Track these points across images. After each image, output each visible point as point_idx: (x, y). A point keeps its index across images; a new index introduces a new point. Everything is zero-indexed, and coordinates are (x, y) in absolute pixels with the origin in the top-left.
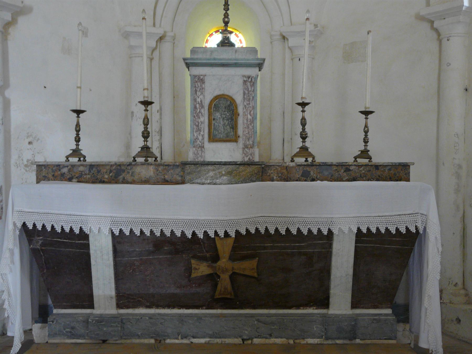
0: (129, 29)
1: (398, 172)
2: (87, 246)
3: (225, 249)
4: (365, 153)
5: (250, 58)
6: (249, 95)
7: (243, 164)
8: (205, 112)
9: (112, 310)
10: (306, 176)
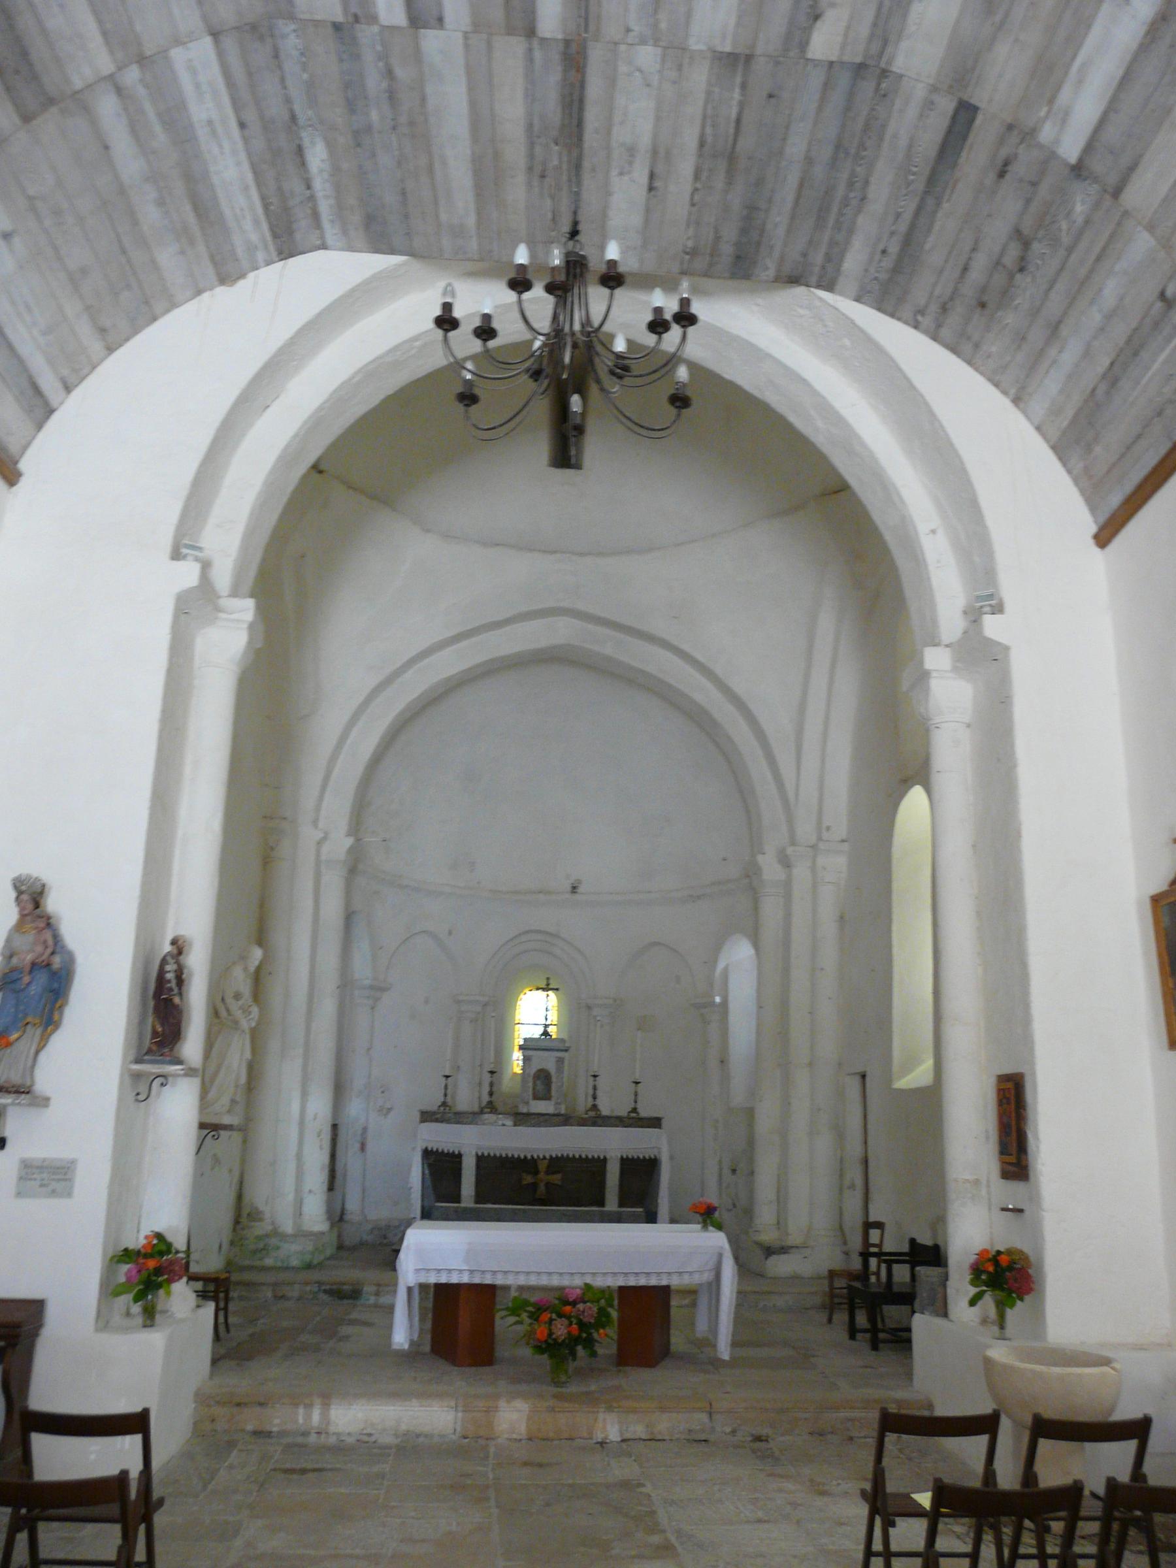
0: (461, 998)
1: (655, 1123)
2: (460, 1163)
3: (542, 1166)
4: (634, 1110)
5: (561, 1046)
6: (560, 1069)
7: (554, 1115)
8: (531, 1079)
9: (472, 1205)
10: (594, 1124)
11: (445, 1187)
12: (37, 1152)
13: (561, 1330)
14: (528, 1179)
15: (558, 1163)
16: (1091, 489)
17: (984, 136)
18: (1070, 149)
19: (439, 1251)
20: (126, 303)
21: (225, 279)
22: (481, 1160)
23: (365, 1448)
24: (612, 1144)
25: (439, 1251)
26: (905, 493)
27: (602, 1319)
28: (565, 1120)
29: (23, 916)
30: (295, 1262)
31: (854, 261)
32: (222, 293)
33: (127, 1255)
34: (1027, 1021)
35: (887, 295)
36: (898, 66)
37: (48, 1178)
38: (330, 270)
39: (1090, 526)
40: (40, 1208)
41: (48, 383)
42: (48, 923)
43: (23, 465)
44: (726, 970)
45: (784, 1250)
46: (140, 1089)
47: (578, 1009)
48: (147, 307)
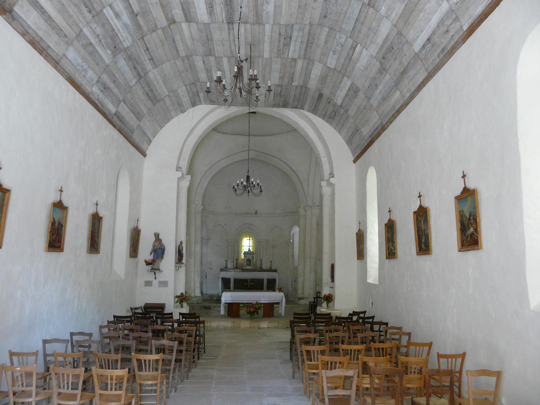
1: (275, 271)
3: (249, 281)
11: (226, 285)
12: (161, 280)
13: (252, 310)
14: (246, 284)
15: (252, 280)
16: (353, 152)
17: (324, 100)
18: (339, 102)
19: (227, 297)
20: (164, 119)
21: (183, 112)
22: (235, 279)
23: (218, 328)
24: (265, 276)
25: (227, 297)
26: (319, 149)
27: (260, 308)
28: (254, 270)
29: (156, 240)
30: (195, 302)
31: (306, 107)
32: (182, 116)
33: (177, 297)
34: (335, 254)
35: (314, 111)
36: (309, 86)
37: (164, 284)
38: (203, 109)
39: (352, 159)
40: (163, 289)
41: (149, 134)
42: (160, 241)
44: (293, 233)
45: (303, 298)
46: (177, 269)
47: (257, 243)
48: (167, 119)
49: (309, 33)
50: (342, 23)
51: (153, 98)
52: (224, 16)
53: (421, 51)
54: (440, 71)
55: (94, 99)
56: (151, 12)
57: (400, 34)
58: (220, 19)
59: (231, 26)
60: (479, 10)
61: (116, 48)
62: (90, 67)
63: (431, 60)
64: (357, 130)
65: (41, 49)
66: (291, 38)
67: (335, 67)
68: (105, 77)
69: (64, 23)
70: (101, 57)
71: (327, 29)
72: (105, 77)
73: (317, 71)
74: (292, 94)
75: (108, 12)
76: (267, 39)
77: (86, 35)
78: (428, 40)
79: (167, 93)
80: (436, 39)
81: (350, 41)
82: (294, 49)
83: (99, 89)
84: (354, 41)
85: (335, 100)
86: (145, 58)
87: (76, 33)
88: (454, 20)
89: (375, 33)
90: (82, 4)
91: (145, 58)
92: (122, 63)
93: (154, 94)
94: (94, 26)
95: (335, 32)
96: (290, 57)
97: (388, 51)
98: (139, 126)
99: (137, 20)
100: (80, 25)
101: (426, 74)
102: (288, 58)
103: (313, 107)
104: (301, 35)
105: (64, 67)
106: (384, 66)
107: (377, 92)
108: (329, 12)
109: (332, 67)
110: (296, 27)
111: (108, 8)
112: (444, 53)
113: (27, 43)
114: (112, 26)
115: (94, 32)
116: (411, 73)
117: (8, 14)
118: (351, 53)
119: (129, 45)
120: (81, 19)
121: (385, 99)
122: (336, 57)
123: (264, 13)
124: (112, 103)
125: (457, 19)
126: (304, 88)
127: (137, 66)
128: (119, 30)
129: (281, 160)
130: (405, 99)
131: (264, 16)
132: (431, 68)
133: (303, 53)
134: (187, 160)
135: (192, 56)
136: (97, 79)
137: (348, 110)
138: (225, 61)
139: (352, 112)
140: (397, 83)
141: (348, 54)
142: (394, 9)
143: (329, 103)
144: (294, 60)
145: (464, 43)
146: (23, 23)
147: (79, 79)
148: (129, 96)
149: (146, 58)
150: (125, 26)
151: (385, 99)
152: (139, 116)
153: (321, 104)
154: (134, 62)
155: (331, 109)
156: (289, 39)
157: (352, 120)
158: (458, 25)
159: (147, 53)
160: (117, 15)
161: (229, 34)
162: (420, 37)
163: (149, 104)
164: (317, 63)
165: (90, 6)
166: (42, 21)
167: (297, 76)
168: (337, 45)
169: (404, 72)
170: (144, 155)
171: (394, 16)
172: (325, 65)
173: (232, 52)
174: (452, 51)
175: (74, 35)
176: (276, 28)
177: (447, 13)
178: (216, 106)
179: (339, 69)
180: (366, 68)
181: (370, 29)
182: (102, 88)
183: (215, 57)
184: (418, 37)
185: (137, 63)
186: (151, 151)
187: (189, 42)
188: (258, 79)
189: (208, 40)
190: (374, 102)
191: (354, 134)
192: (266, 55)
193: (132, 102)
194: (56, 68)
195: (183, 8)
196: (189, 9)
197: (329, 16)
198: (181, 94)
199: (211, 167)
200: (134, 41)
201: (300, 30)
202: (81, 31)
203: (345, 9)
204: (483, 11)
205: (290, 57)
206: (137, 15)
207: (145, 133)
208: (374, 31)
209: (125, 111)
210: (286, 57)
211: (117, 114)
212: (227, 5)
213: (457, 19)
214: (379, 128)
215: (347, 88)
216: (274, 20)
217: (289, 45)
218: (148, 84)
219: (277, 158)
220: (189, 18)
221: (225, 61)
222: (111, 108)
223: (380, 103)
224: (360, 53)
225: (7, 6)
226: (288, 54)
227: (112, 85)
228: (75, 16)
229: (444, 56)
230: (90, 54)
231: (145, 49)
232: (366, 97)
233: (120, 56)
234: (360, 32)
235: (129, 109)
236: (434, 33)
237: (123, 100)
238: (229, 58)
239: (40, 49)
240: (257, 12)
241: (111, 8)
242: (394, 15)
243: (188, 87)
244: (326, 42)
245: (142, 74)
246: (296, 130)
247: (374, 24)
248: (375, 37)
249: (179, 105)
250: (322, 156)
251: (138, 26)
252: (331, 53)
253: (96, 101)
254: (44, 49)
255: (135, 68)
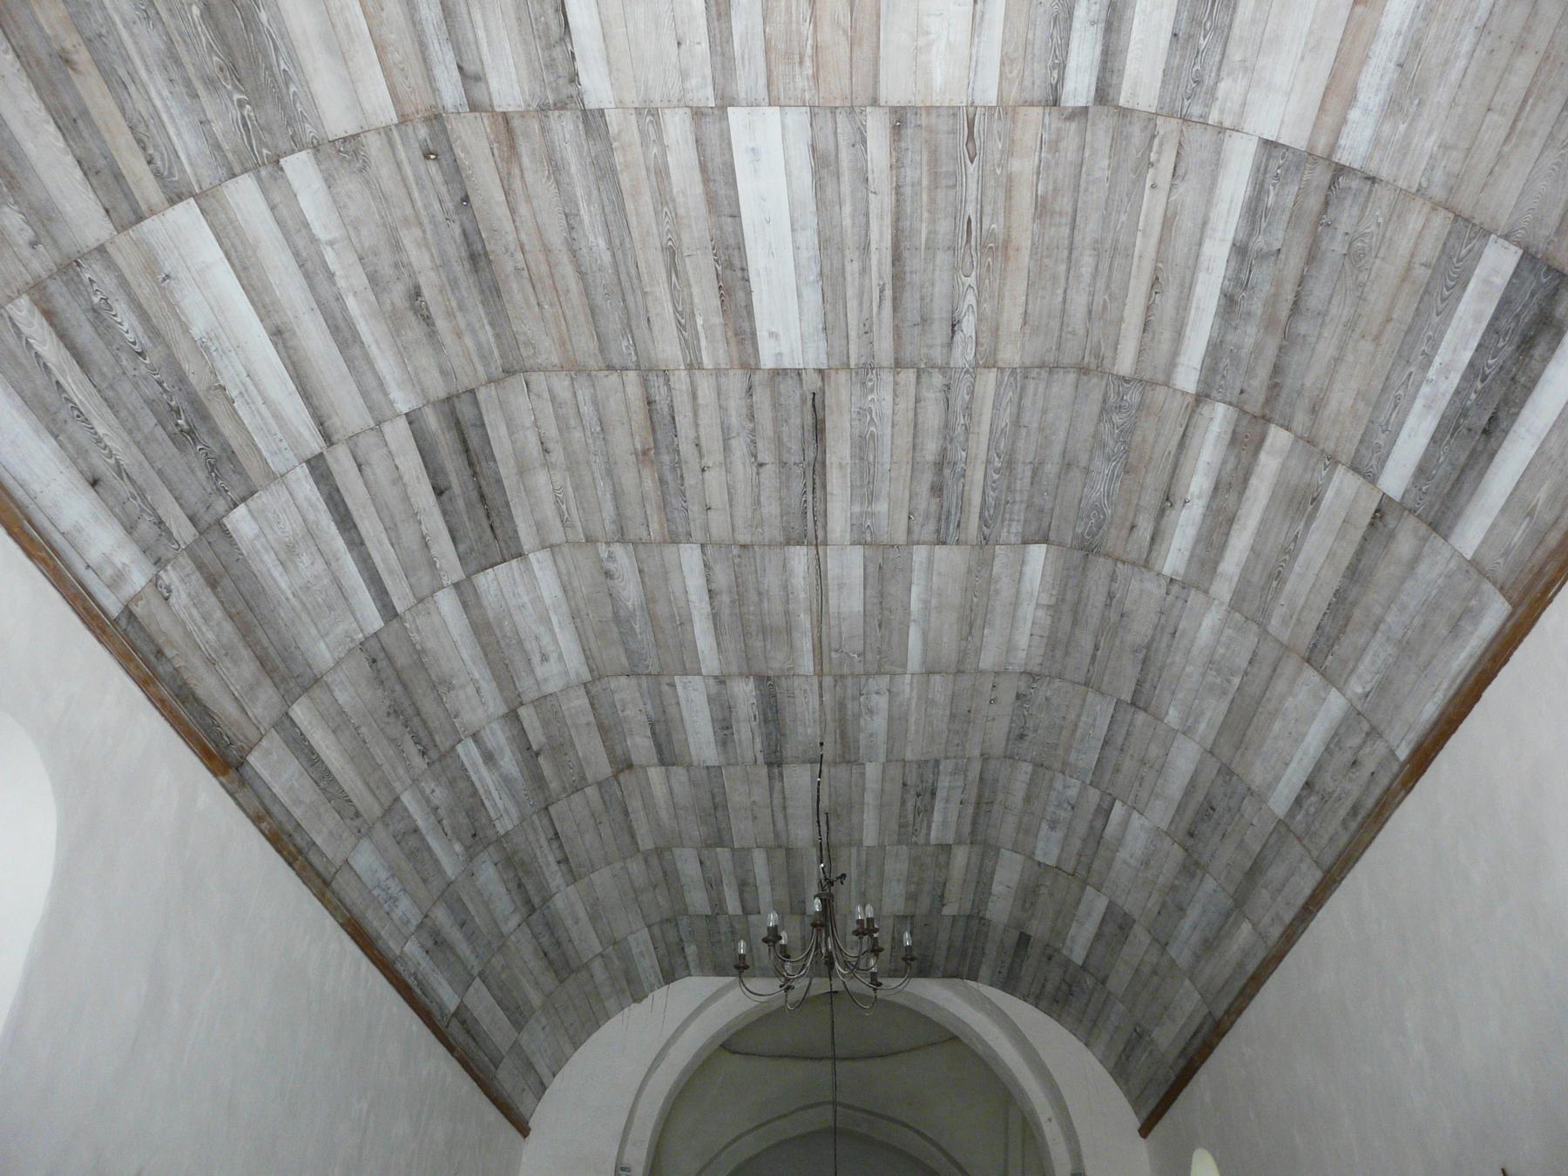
16: (1135, 1104)
17: (1034, 951)
18: (1078, 956)
21: (637, 998)
31: (984, 971)
32: (635, 1010)
35: (1009, 983)
36: (988, 916)
39: (1134, 1123)
41: (542, 1068)
43: (531, 1124)
48: (593, 1020)
49: (981, 778)
50: (1068, 749)
51: (560, 961)
52: (758, 746)
53: (1291, 813)
54: (1358, 866)
55: (405, 975)
56: (572, 744)
57: (1226, 771)
58: (749, 755)
59: (776, 770)
60: (1429, 710)
61: (476, 835)
62: (405, 890)
63: (1327, 837)
64: (1140, 1036)
65: (293, 849)
66: (933, 794)
67: (1059, 860)
68: (441, 915)
69: (359, 784)
70: (436, 862)
71: (1027, 768)
72: (441, 915)
73: (1008, 874)
74: (944, 936)
75: (468, 752)
76: (870, 799)
77: (406, 809)
78: (1308, 785)
79: (599, 949)
80: (1327, 781)
81: (1094, 796)
82: (943, 822)
83: (422, 946)
84: (1104, 792)
85: (1064, 952)
86: (548, 859)
87: (381, 804)
88: (1368, 734)
89: (1159, 773)
90: (408, 737)
91: (548, 859)
92: (489, 874)
93: (564, 954)
94: (428, 785)
95: (1049, 774)
96: (933, 841)
97: (1201, 818)
98: (516, 1044)
99: (538, 766)
100: (398, 786)
101: (1319, 875)
102: (927, 844)
103: (1005, 971)
104: (961, 783)
105: (342, 894)
106: (1195, 856)
107: (1186, 925)
108: (1030, 724)
109: (1051, 861)
110: (947, 766)
111: (470, 742)
112: (1359, 818)
113: (263, 838)
114: (473, 784)
115: (428, 801)
116: (1276, 872)
117: (232, 773)
118: (1098, 824)
119: (510, 827)
120: (401, 771)
121: (1210, 945)
122: (1058, 835)
123: (862, 736)
124: (450, 984)
125: (1374, 733)
126: (975, 921)
127: (524, 880)
128: (488, 792)
129: (918, 1132)
130: (1270, 943)
131: (862, 743)
132: (1328, 859)
133: (967, 828)
134: (646, 1145)
135: (669, 849)
136: (420, 917)
137: (1107, 977)
138: (759, 857)
139: (1119, 980)
140: (1240, 901)
141: (1091, 827)
142: (1202, 713)
143: (1050, 958)
144: (946, 849)
145: (1408, 792)
146: (262, 790)
147: (374, 922)
148: (497, 962)
149: (551, 858)
150: (506, 780)
151: (1210, 945)
152: (518, 1015)
153: (1024, 963)
154: (518, 869)
155: (1055, 975)
156: (928, 795)
157: (1120, 1007)
158: (1380, 748)
159: (555, 845)
160: (489, 758)
161: (771, 789)
162: (1284, 779)
163: (548, 981)
164: (1006, 854)
165: (425, 740)
166: (308, 782)
167: (953, 890)
168: (1059, 805)
169: (1255, 871)
170: (523, 1130)
171: (1205, 728)
172: (1030, 857)
173: (776, 834)
174: (1380, 813)
175: (377, 811)
176: (895, 771)
177: (1345, 718)
178: (728, 979)
179: (1069, 866)
180: (1146, 864)
181: (1143, 762)
182: (429, 944)
183: (733, 850)
184: (1278, 779)
185: (527, 872)
186: (543, 1117)
187: (664, 815)
188: (876, 931)
189: (715, 808)
190: (1181, 953)
191: (1133, 1049)
192: (870, 838)
193: (503, 976)
194: (321, 897)
195: (654, 734)
196: (669, 735)
197: (1031, 735)
198: (635, 951)
199: (711, 1161)
200: (523, 819)
201: (954, 773)
202: (397, 799)
203: (1072, 716)
204: (1442, 714)
205: (933, 841)
206: (538, 754)
207: (530, 1065)
208: (1157, 767)
209: (482, 1003)
210: (921, 839)
211: (461, 1014)
212: (766, 721)
213: (1374, 733)
214: (1205, 1030)
215: (1096, 917)
216: (889, 752)
217: (929, 811)
218: (550, 926)
219: (905, 1125)
220: (667, 754)
221: (759, 857)
222: (447, 996)
223: (1198, 958)
224: (1125, 823)
225: (234, 753)
226: (928, 834)
227: (455, 935)
228: (386, 767)
229: (1361, 826)
230: (412, 855)
231: (551, 835)
232: (1155, 940)
233: (484, 856)
234: (1117, 770)
235: (494, 996)
236: (1319, 767)
237: (480, 975)
238: (769, 851)
239: (290, 853)
240: (843, 735)
241: (476, 742)
242: (1202, 727)
243: (656, 929)
244: (1028, 799)
245: (536, 901)
246: (954, 1038)
247: (1154, 751)
248: (1160, 781)
249: (629, 982)
250: (1043, 1119)
251: (538, 780)
252: (1045, 826)
253: (411, 981)
254: (300, 852)
255: (520, 886)
